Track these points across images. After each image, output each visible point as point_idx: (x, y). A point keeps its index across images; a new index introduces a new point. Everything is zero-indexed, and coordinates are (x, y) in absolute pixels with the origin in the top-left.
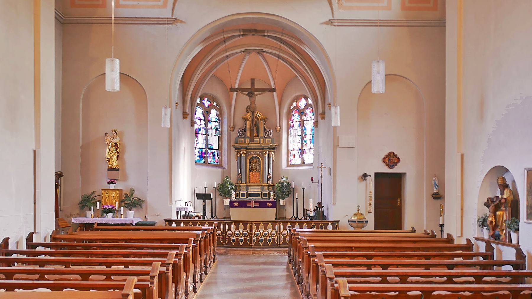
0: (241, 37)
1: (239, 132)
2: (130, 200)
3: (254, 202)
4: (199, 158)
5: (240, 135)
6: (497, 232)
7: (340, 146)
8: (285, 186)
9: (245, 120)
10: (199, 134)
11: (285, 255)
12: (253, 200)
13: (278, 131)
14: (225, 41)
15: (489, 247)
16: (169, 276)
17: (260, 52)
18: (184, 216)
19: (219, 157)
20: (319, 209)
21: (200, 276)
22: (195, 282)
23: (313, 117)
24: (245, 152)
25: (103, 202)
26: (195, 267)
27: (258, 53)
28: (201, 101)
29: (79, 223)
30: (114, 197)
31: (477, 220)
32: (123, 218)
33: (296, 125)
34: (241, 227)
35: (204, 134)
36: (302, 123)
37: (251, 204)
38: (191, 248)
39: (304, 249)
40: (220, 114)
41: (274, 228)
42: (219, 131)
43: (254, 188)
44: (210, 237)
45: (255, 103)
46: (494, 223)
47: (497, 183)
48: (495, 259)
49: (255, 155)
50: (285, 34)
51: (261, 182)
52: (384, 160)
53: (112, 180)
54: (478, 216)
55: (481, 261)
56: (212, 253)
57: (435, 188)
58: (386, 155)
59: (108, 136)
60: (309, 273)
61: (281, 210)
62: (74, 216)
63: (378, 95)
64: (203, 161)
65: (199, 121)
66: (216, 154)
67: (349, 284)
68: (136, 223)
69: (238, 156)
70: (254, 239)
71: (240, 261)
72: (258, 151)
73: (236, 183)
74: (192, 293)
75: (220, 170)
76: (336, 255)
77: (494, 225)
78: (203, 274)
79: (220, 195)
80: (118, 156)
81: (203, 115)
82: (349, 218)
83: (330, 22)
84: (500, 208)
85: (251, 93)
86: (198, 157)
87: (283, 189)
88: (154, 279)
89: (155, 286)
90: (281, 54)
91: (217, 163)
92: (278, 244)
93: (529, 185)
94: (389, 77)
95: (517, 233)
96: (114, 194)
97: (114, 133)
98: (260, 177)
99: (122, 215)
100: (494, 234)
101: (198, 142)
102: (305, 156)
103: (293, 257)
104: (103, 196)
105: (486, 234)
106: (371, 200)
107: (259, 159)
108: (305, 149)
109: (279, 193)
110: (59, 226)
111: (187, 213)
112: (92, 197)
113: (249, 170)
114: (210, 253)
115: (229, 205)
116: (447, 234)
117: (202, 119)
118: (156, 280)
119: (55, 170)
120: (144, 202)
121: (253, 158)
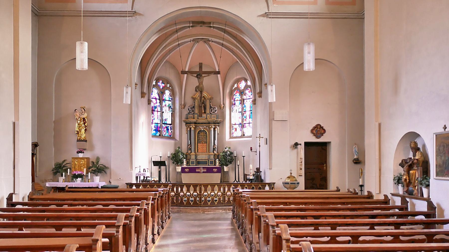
0: (191, 28)
1: (189, 109)
2: (96, 167)
3: (200, 172)
4: (155, 132)
5: (189, 112)
6: (411, 188)
7: (275, 120)
8: (228, 155)
9: (194, 99)
10: (155, 111)
11: (229, 213)
12: (201, 166)
13: (222, 108)
14: (177, 31)
15: (404, 201)
16: (132, 227)
17: (206, 41)
18: (143, 181)
19: (171, 131)
20: (257, 173)
21: (157, 229)
22: (153, 234)
23: (251, 96)
24: (194, 126)
25: (73, 169)
26: (153, 222)
27: (205, 42)
28: (156, 83)
29: (52, 187)
30: (83, 165)
31: (392, 178)
32: (90, 182)
33: (237, 103)
34: (192, 188)
35: (159, 111)
36: (242, 102)
37: (199, 170)
38: (150, 204)
39: (248, 204)
40: (173, 94)
41: (220, 190)
42: (171, 108)
43: (202, 157)
44: (166, 197)
45: (202, 83)
46: (408, 181)
47: (410, 146)
48: (409, 210)
49: (202, 128)
50: (228, 25)
51: (208, 152)
52: (312, 131)
53: (81, 150)
54: (394, 175)
55: (397, 212)
56: (167, 210)
57: (355, 154)
58: (314, 127)
59: (77, 112)
60: (252, 224)
61: (225, 175)
62: (48, 181)
63: (309, 72)
64: (158, 134)
65: (155, 100)
66: (169, 128)
67: (289, 228)
68: (101, 186)
69: (188, 129)
70: (202, 199)
71: (192, 218)
72: (205, 126)
73: (186, 153)
74: (151, 244)
75: (172, 142)
76: (275, 209)
77: (408, 182)
78: (160, 228)
79: (173, 163)
80: (86, 130)
81: (158, 95)
82: (283, 180)
83: (266, 15)
84: (413, 168)
85: (199, 75)
86: (154, 130)
87: (227, 157)
88: (119, 228)
89: (120, 235)
90: (224, 43)
91: (170, 136)
92: (223, 203)
93: (437, 147)
94: (318, 61)
95: (428, 189)
96: (83, 162)
97: (83, 109)
98: (207, 147)
99: (90, 180)
100: (408, 190)
101: (154, 118)
102: (245, 130)
103: (237, 213)
104: (73, 163)
105: (401, 190)
106: (301, 165)
107: (206, 132)
108: (245, 124)
109: (223, 161)
110: (35, 189)
111: (145, 178)
112: (64, 164)
113: (198, 141)
114: (166, 211)
115: (180, 171)
116: (368, 191)
117: (157, 98)
118: (121, 229)
119: (32, 141)
120: (108, 168)
121: (201, 131)
